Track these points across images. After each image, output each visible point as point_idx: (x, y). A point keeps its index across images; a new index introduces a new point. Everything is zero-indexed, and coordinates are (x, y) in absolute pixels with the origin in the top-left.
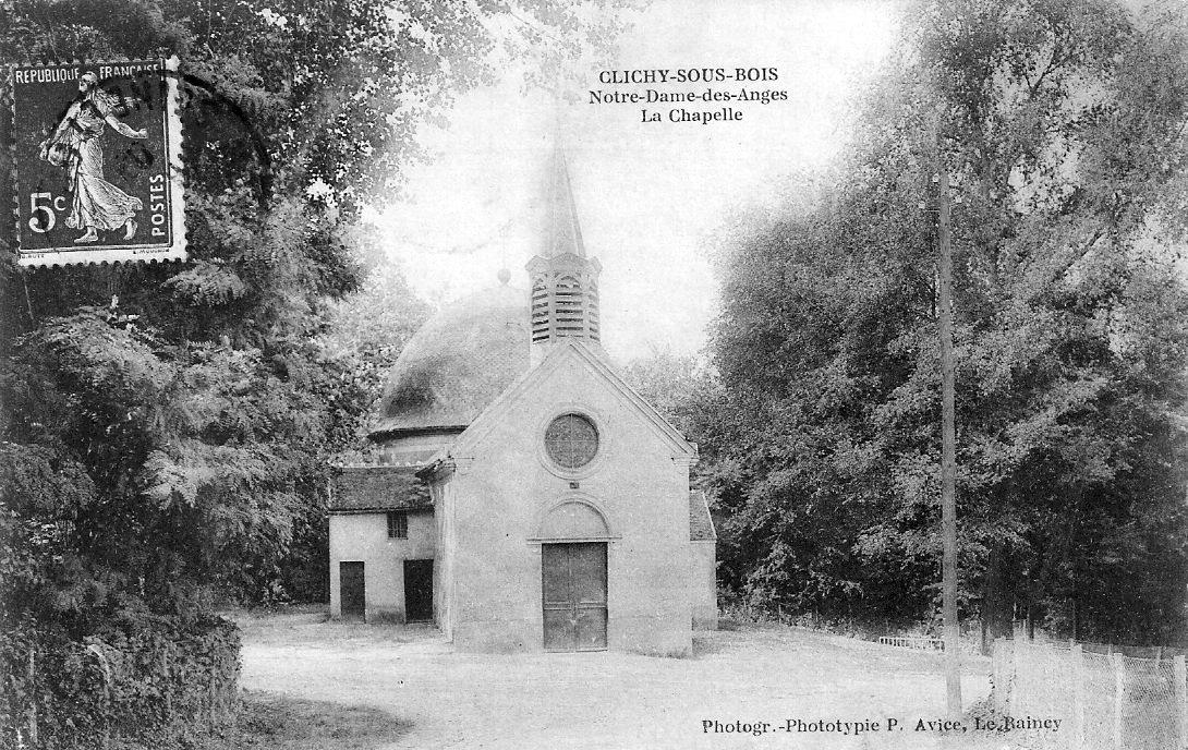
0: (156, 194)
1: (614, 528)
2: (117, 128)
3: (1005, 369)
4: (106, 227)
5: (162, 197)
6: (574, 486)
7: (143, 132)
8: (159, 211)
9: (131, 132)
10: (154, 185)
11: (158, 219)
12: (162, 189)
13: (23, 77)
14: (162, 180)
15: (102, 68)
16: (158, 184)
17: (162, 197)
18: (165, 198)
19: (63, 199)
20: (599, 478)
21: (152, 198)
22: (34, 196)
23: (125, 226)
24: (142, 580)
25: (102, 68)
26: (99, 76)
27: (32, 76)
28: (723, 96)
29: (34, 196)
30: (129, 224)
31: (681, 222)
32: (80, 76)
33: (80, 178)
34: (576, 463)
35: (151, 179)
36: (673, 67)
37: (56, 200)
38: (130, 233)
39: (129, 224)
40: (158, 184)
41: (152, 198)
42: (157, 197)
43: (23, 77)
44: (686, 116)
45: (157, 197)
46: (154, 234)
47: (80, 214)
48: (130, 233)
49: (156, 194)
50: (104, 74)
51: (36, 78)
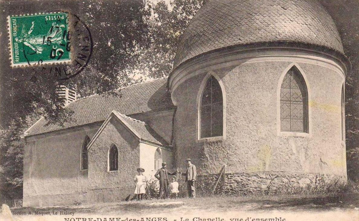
4: (61, 33)
5: (52, 17)
7: (33, 23)
8: (56, 17)
10: (48, 19)
14: (47, 17)
15: (14, 36)
16: (48, 18)
22: (13, 65)
24: (23, 106)
27: (17, 57)
29: (13, 65)
36: (154, 159)
40: (48, 18)
42: (52, 18)
46: (63, 18)
47: (58, 41)
49: (51, 18)
50: (16, 35)
51: (18, 56)
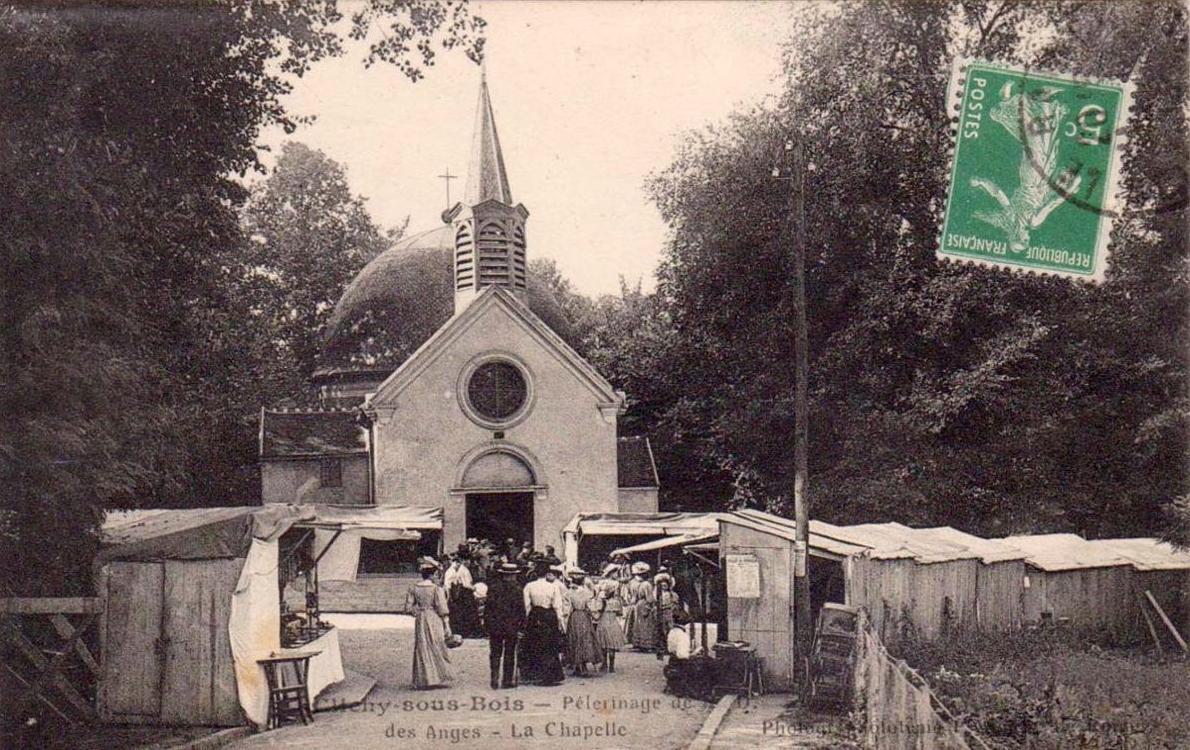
0: (975, 120)
1: (539, 478)
2: (1000, 192)
3: (945, 316)
5: (970, 115)
6: (500, 435)
9: (988, 186)
11: (977, 94)
12: (968, 124)
13: (1082, 259)
16: (970, 130)
17: (970, 115)
18: (966, 114)
19: (1067, 133)
20: (525, 431)
21: (979, 117)
23: (1012, 94)
25: (1004, 253)
26: (1008, 247)
27: (1073, 259)
28: (407, 733)
30: (1007, 95)
31: (106, 479)
32: (1027, 250)
33: (1046, 150)
34: (504, 414)
35: (976, 135)
37: (1073, 134)
38: (1007, 89)
39: (1007, 95)
41: (979, 117)
42: (975, 116)
43: (1082, 259)
44: (565, 730)
45: (975, 116)
48: (1007, 89)
49: (975, 120)
51: (1071, 256)
